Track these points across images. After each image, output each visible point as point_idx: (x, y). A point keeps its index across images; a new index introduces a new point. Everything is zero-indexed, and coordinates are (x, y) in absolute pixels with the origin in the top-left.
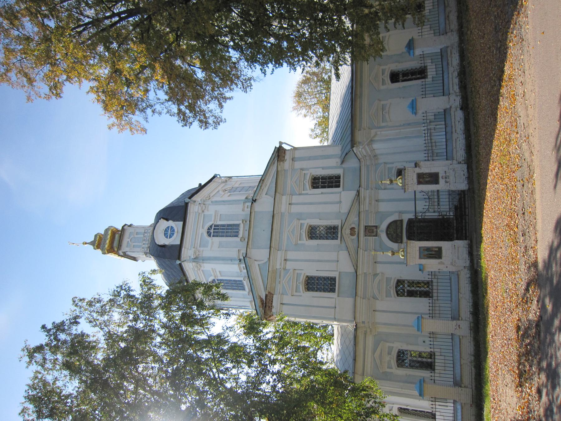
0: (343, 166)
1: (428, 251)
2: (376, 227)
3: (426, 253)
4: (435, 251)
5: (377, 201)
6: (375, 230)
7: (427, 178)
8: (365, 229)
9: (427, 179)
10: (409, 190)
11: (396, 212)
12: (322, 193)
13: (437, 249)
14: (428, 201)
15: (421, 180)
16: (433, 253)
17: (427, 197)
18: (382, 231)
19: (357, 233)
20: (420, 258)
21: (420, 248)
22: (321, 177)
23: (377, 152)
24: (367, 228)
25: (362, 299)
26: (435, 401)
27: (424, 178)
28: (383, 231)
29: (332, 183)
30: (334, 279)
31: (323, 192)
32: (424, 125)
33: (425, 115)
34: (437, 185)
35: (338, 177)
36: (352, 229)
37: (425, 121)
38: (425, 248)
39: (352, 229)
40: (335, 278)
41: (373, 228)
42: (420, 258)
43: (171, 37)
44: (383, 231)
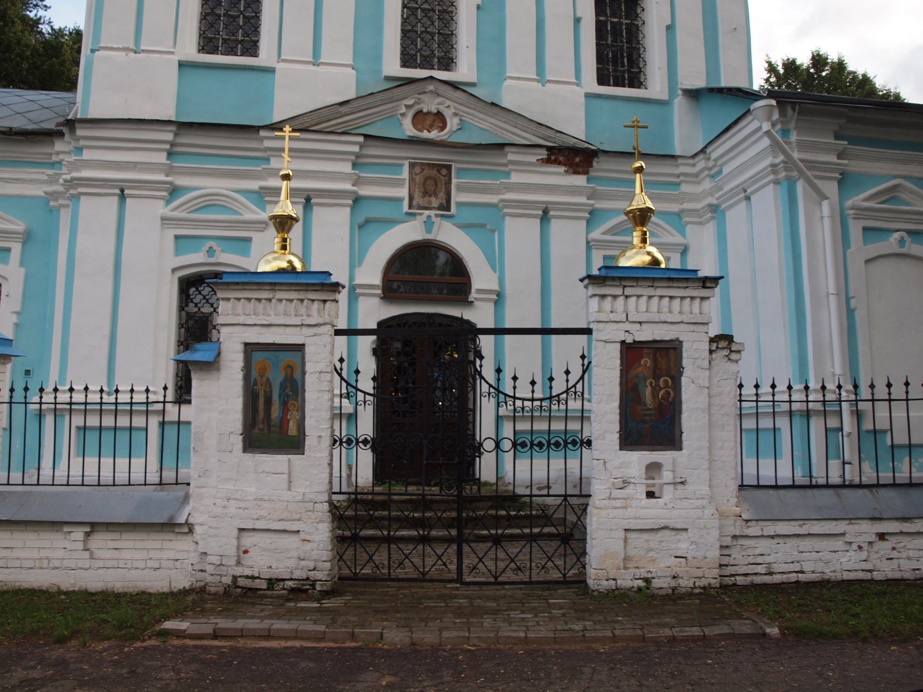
0: (679, 102)
1: (283, 386)
2: (446, 206)
3: (277, 378)
4: (284, 421)
5: (545, 217)
6: (435, 202)
7: (654, 395)
8: (439, 167)
9: (648, 390)
10: (594, 302)
11: (501, 282)
12: (577, 21)
13: (293, 430)
14: (538, 395)
15: (647, 361)
16: (276, 412)
17: (559, 387)
18: (428, 224)
19: (425, 134)
20: (250, 349)
21: (299, 348)
22: (640, 23)
23: (736, 216)
24: (444, 172)
25: (167, 147)
26: (11, 403)
27: (656, 377)
28: (429, 231)
29: (615, 61)
30: (252, 49)
31: (583, 24)
32: (799, 386)
33: (898, 391)
34: (614, 438)
35: (636, 81)
36: (439, 119)
37: (865, 393)
38: (297, 375)
39: (439, 119)
40: (255, 54)
41: (442, 195)
42: (250, 349)
43: (439, 514)
44: (429, 231)
